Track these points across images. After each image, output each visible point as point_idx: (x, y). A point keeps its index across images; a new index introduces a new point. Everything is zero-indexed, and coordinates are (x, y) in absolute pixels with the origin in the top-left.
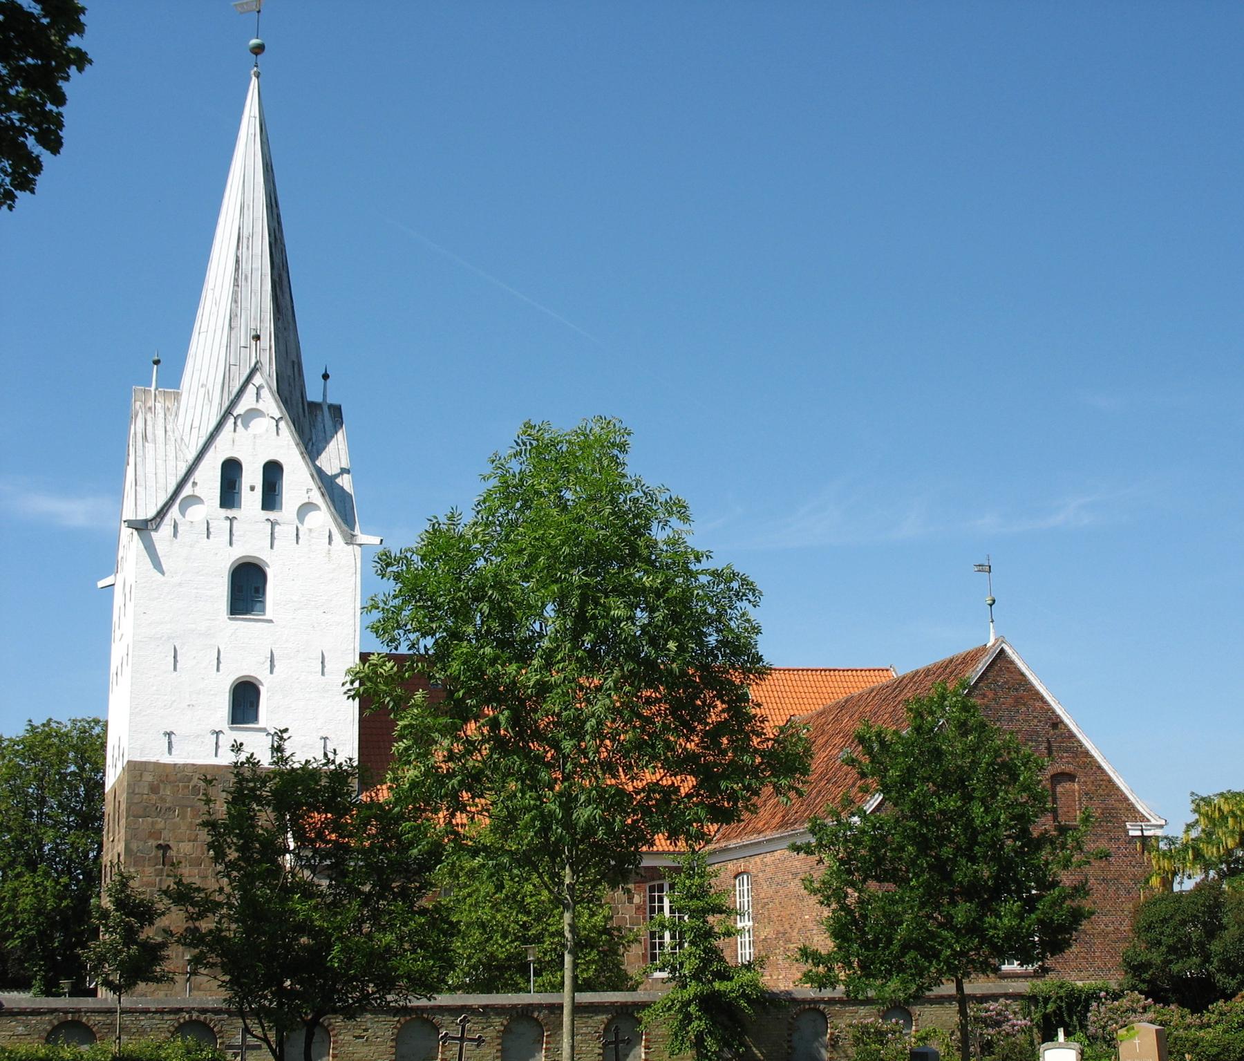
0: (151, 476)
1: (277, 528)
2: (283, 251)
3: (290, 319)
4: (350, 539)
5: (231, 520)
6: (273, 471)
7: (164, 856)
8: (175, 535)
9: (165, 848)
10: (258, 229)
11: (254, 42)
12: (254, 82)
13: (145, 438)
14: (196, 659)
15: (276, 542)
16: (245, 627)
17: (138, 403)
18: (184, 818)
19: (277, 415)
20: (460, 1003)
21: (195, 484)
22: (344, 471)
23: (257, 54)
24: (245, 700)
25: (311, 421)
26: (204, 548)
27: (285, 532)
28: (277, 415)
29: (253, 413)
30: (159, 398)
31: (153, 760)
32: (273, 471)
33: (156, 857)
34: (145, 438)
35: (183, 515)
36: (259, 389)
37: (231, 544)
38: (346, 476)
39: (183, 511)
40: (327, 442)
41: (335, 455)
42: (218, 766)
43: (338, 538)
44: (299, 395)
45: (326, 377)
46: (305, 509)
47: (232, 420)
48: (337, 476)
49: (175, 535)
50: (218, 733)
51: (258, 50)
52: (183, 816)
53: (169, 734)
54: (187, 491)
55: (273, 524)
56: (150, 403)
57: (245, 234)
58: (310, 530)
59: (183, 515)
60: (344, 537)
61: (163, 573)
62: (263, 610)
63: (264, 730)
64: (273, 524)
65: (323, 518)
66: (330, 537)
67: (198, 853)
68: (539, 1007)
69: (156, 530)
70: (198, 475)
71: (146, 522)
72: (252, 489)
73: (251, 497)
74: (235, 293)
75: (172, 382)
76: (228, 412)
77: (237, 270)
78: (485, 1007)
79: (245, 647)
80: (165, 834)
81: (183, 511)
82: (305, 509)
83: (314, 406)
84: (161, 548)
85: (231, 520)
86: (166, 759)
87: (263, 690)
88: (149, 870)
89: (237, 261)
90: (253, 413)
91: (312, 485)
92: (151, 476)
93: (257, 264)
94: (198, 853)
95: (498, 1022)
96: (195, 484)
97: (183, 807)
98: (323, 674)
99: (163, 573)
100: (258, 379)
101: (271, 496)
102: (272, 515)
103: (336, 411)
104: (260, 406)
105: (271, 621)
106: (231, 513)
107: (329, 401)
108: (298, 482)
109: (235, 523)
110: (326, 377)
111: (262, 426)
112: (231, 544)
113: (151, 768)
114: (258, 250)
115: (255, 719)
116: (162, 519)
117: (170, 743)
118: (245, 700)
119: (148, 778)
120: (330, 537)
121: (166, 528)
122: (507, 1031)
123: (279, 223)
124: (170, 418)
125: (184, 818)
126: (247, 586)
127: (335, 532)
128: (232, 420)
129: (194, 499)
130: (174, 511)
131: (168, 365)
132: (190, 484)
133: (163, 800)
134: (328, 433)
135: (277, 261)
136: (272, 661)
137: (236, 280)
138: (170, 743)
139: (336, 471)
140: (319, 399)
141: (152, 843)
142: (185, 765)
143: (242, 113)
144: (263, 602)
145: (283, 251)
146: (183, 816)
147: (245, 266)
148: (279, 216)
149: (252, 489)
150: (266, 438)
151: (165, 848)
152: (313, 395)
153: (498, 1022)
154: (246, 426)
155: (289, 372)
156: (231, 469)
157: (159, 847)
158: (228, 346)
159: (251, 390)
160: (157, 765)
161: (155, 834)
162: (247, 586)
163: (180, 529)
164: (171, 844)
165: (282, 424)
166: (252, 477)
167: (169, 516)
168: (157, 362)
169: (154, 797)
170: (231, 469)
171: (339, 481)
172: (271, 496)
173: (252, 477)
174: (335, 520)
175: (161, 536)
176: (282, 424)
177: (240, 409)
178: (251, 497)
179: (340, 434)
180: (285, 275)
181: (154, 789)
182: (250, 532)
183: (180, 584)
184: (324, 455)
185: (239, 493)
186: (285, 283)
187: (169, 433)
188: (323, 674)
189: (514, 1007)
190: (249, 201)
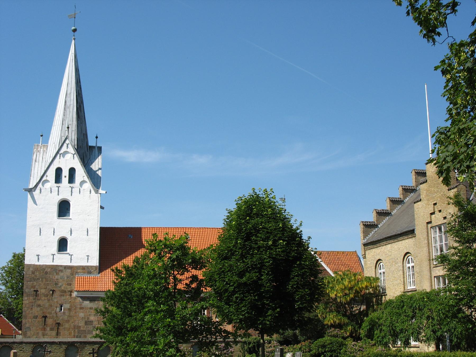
0: (36, 173)
1: (73, 189)
2: (82, 97)
3: (83, 120)
4: (97, 192)
5: (58, 187)
6: (72, 171)
7: (36, 293)
8: (40, 193)
9: (36, 291)
10: (73, 91)
11: (73, 28)
12: (73, 41)
13: (36, 161)
14: (47, 232)
15: (73, 194)
16: (63, 221)
17: (35, 149)
18: (42, 282)
19: (74, 153)
20: (52, 341)
21: (47, 176)
22: (100, 169)
23: (74, 32)
24: (63, 244)
25: (86, 152)
26: (49, 197)
27: (76, 190)
28: (74, 153)
29: (66, 153)
30: (42, 148)
31: (33, 263)
32: (72, 171)
33: (34, 294)
34: (36, 161)
35: (43, 186)
36: (67, 145)
37: (58, 195)
38: (100, 171)
39: (43, 185)
40: (95, 159)
41: (96, 165)
42: (54, 265)
43: (93, 191)
44: (86, 144)
45: (97, 137)
46: (82, 183)
47: (59, 155)
48: (97, 171)
49: (40, 193)
50: (53, 255)
51: (75, 31)
52: (42, 281)
53: (38, 256)
54: (44, 178)
55: (72, 188)
56: (39, 149)
57: (68, 93)
58: (84, 189)
59: (43, 186)
60: (95, 191)
61: (37, 205)
62: (69, 215)
63: (68, 253)
64: (72, 188)
65: (88, 185)
66: (90, 191)
67: (47, 293)
68: (77, 342)
69: (34, 191)
70: (48, 173)
71: (31, 189)
72: (65, 177)
73: (65, 180)
74: (64, 112)
75: (46, 142)
76: (58, 152)
77: (65, 105)
78: (60, 342)
79: (62, 227)
80: (37, 287)
81: (43, 185)
82: (82, 183)
83: (92, 148)
84: (36, 197)
85: (58, 187)
86: (52, 264)
87: (68, 241)
88: (31, 298)
89: (65, 102)
90: (66, 153)
91: (84, 175)
92: (36, 173)
93: (72, 103)
94: (47, 293)
95: (64, 347)
96: (47, 176)
97: (42, 278)
98: (87, 235)
99: (37, 205)
100: (67, 142)
101: (71, 179)
102: (71, 185)
103: (100, 148)
104: (68, 150)
105: (71, 219)
106: (58, 185)
107: (98, 146)
108: (81, 174)
109: (60, 188)
110: (97, 137)
111: (69, 156)
112: (58, 195)
113: (32, 266)
114: (72, 98)
115: (66, 250)
116: (36, 188)
117: (38, 258)
118: (63, 244)
119: (31, 269)
120: (90, 191)
121: (38, 191)
122: (66, 350)
123: (81, 88)
124: (45, 154)
125: (42, 282)
126: (64, 208)
127: (92, 189)
128: (59, 155)
129: (47, 181)
130: (40, 185)
131: (44, 136)
132: (45, 176)
133: (36, 276)
134: (96, 156)
135: (79, 101)
136: (54, 233)
137: (65, 108)
138: (38, 258)
139: (97, 169)
140: (94, 145)
141: (32, 289)
142: (43, 265)
143: (69, 52)
144: (69, 213)
145: (82, 97)
146: (42, 281)
147: (68, 103)
148: (80, 86)
149: (65, 177)
150: (71, 160)
151: (36, 291)
152: (92, 142)
153: (64, 347)
154: (64, 157)
155: (82, 138)
156: (59, 171)
157: (35, 291)
158: (62, 130)
159: (65, 145)
160: (34, 265)
161: (34, 287)
162: (64, 208)
163: (42, 191)
164: (38, 290)
165: (75, 156)
166: (65, 173)
167: (38, 187)
168: (42, 136)
169: (33, 275)
170: (59, 171)
171: (97, 172)
172: (71, 179)
173: (65, 173)
174: (92, 186)
175: (36, 193)
176: (75, 156)
177: (62, 151)
178: (65, 180)
179: (100, 157)
180: (82, 105)
181: (33, 273)
182: (64, 190)
183: (42, 208)
184: (94, 164)
185: (62, 178)
186: (82, 108)
187: (44, 159)
188: (87, 235)
189: (69, 342)
190: (70, 82)
